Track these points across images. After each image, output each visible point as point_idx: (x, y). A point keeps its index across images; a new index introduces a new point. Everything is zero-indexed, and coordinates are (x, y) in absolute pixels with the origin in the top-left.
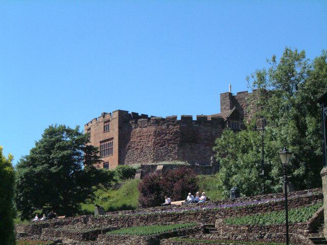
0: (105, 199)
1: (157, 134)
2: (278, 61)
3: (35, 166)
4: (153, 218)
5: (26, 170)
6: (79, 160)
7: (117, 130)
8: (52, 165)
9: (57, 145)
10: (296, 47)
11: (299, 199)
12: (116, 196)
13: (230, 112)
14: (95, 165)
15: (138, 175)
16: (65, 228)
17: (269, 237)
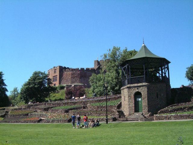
0: (54, 96)
1: (72, 74)
2: (111, 50)
3: (30, 85)
4: (67, 103)
5: (27, 86)
6: (45, 83)
7: (59, 73)
8: (36, 85)
9: (37, 78)
10: (117, 46)
11: (115, 97)
12: (58, 95)
13: (97, 67)
14: (50, 85)
15: (65, 88)
16: (38, 106)
17: (104, 110)
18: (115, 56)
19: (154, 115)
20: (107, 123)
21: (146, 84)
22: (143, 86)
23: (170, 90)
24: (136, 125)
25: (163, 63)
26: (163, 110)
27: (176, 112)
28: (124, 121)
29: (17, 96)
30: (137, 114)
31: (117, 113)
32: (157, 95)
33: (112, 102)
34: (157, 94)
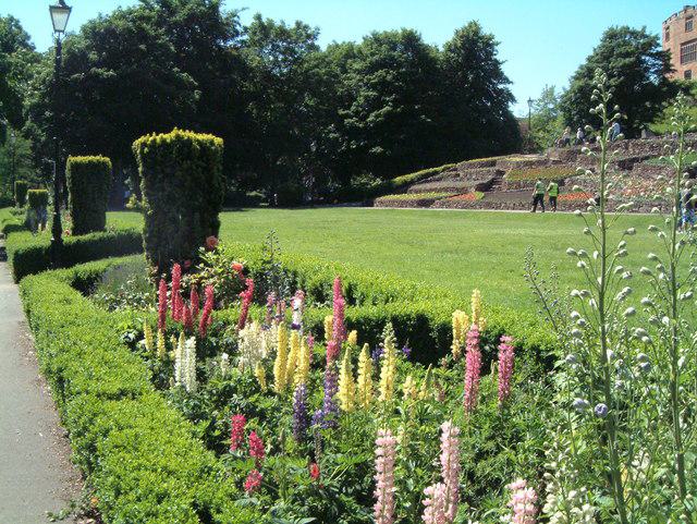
5: (581, 83)
14: (667, 75)
29: (554, 119)
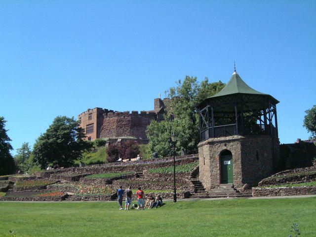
0: (89, 158)
1: (118, 121)
2: (182, 82)
3: (49, 139)
4: (110, 169)
5: (44, 141)
6: (74, 136)
7: (96, 119)
8: (58, 138)
9: (61, 127)
10: (192, 75)
11: (188, 159)
12: (94, 156)
13: (160, 109)
14: (82, 139)
15: (107, 145)
16: (62, 174)
17: (170, 180)
18: (188, 92)
19: (253, 188)
20: (175, 201)
21: (240, 137)
22: (233, 141)
23: (279, 147)
24: (223, 204)
25: (267, 102)
26: (266, 179)
27: (289, 184)
28: (203, 197)
29: (28, 158)
30: (225, 187)
31: (192, 185)
32: (257, 155)
33: (183, 166)
34: (257, 153)
